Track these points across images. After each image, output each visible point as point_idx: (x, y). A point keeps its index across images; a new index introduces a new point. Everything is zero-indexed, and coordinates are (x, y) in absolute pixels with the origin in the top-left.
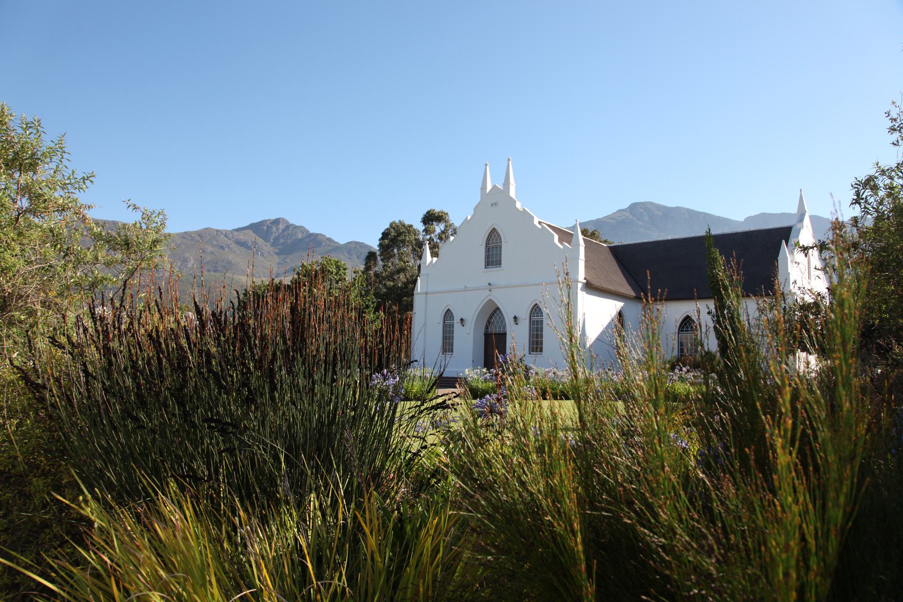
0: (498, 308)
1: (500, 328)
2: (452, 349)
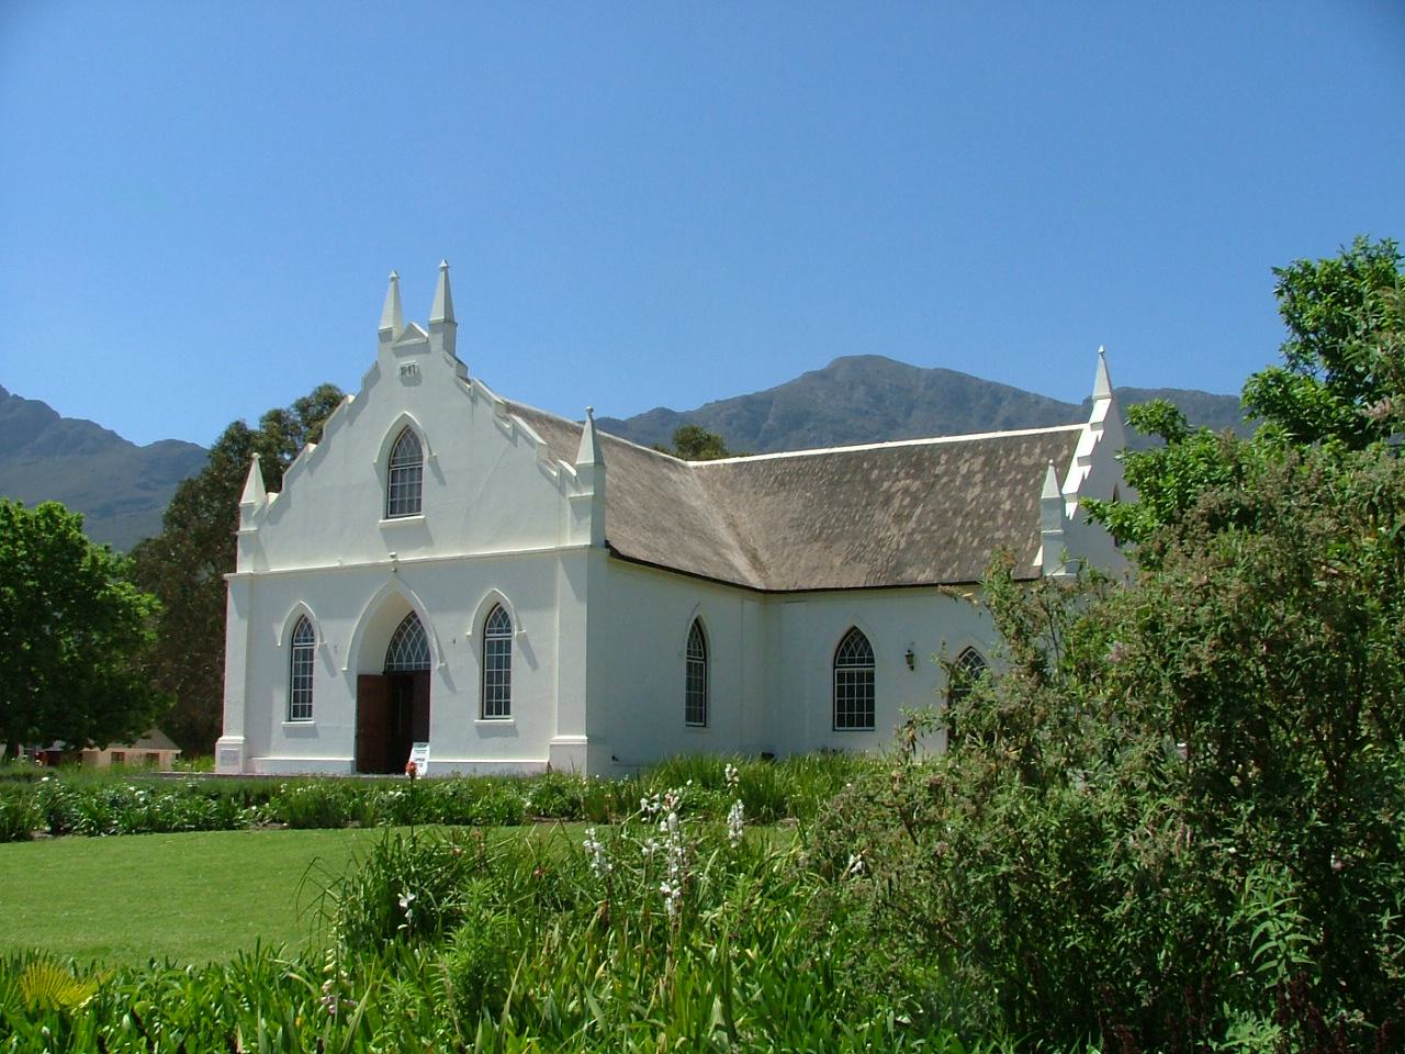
0: (413, 614)
1: (418, 659)
2: (507, 705)
